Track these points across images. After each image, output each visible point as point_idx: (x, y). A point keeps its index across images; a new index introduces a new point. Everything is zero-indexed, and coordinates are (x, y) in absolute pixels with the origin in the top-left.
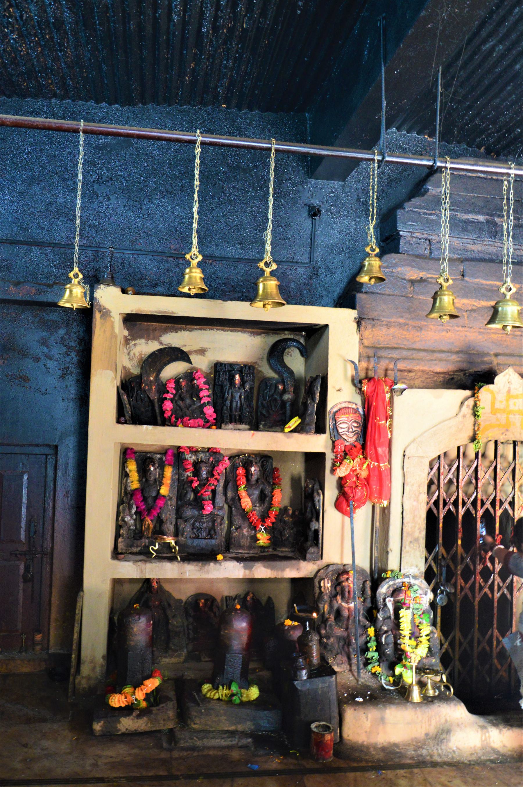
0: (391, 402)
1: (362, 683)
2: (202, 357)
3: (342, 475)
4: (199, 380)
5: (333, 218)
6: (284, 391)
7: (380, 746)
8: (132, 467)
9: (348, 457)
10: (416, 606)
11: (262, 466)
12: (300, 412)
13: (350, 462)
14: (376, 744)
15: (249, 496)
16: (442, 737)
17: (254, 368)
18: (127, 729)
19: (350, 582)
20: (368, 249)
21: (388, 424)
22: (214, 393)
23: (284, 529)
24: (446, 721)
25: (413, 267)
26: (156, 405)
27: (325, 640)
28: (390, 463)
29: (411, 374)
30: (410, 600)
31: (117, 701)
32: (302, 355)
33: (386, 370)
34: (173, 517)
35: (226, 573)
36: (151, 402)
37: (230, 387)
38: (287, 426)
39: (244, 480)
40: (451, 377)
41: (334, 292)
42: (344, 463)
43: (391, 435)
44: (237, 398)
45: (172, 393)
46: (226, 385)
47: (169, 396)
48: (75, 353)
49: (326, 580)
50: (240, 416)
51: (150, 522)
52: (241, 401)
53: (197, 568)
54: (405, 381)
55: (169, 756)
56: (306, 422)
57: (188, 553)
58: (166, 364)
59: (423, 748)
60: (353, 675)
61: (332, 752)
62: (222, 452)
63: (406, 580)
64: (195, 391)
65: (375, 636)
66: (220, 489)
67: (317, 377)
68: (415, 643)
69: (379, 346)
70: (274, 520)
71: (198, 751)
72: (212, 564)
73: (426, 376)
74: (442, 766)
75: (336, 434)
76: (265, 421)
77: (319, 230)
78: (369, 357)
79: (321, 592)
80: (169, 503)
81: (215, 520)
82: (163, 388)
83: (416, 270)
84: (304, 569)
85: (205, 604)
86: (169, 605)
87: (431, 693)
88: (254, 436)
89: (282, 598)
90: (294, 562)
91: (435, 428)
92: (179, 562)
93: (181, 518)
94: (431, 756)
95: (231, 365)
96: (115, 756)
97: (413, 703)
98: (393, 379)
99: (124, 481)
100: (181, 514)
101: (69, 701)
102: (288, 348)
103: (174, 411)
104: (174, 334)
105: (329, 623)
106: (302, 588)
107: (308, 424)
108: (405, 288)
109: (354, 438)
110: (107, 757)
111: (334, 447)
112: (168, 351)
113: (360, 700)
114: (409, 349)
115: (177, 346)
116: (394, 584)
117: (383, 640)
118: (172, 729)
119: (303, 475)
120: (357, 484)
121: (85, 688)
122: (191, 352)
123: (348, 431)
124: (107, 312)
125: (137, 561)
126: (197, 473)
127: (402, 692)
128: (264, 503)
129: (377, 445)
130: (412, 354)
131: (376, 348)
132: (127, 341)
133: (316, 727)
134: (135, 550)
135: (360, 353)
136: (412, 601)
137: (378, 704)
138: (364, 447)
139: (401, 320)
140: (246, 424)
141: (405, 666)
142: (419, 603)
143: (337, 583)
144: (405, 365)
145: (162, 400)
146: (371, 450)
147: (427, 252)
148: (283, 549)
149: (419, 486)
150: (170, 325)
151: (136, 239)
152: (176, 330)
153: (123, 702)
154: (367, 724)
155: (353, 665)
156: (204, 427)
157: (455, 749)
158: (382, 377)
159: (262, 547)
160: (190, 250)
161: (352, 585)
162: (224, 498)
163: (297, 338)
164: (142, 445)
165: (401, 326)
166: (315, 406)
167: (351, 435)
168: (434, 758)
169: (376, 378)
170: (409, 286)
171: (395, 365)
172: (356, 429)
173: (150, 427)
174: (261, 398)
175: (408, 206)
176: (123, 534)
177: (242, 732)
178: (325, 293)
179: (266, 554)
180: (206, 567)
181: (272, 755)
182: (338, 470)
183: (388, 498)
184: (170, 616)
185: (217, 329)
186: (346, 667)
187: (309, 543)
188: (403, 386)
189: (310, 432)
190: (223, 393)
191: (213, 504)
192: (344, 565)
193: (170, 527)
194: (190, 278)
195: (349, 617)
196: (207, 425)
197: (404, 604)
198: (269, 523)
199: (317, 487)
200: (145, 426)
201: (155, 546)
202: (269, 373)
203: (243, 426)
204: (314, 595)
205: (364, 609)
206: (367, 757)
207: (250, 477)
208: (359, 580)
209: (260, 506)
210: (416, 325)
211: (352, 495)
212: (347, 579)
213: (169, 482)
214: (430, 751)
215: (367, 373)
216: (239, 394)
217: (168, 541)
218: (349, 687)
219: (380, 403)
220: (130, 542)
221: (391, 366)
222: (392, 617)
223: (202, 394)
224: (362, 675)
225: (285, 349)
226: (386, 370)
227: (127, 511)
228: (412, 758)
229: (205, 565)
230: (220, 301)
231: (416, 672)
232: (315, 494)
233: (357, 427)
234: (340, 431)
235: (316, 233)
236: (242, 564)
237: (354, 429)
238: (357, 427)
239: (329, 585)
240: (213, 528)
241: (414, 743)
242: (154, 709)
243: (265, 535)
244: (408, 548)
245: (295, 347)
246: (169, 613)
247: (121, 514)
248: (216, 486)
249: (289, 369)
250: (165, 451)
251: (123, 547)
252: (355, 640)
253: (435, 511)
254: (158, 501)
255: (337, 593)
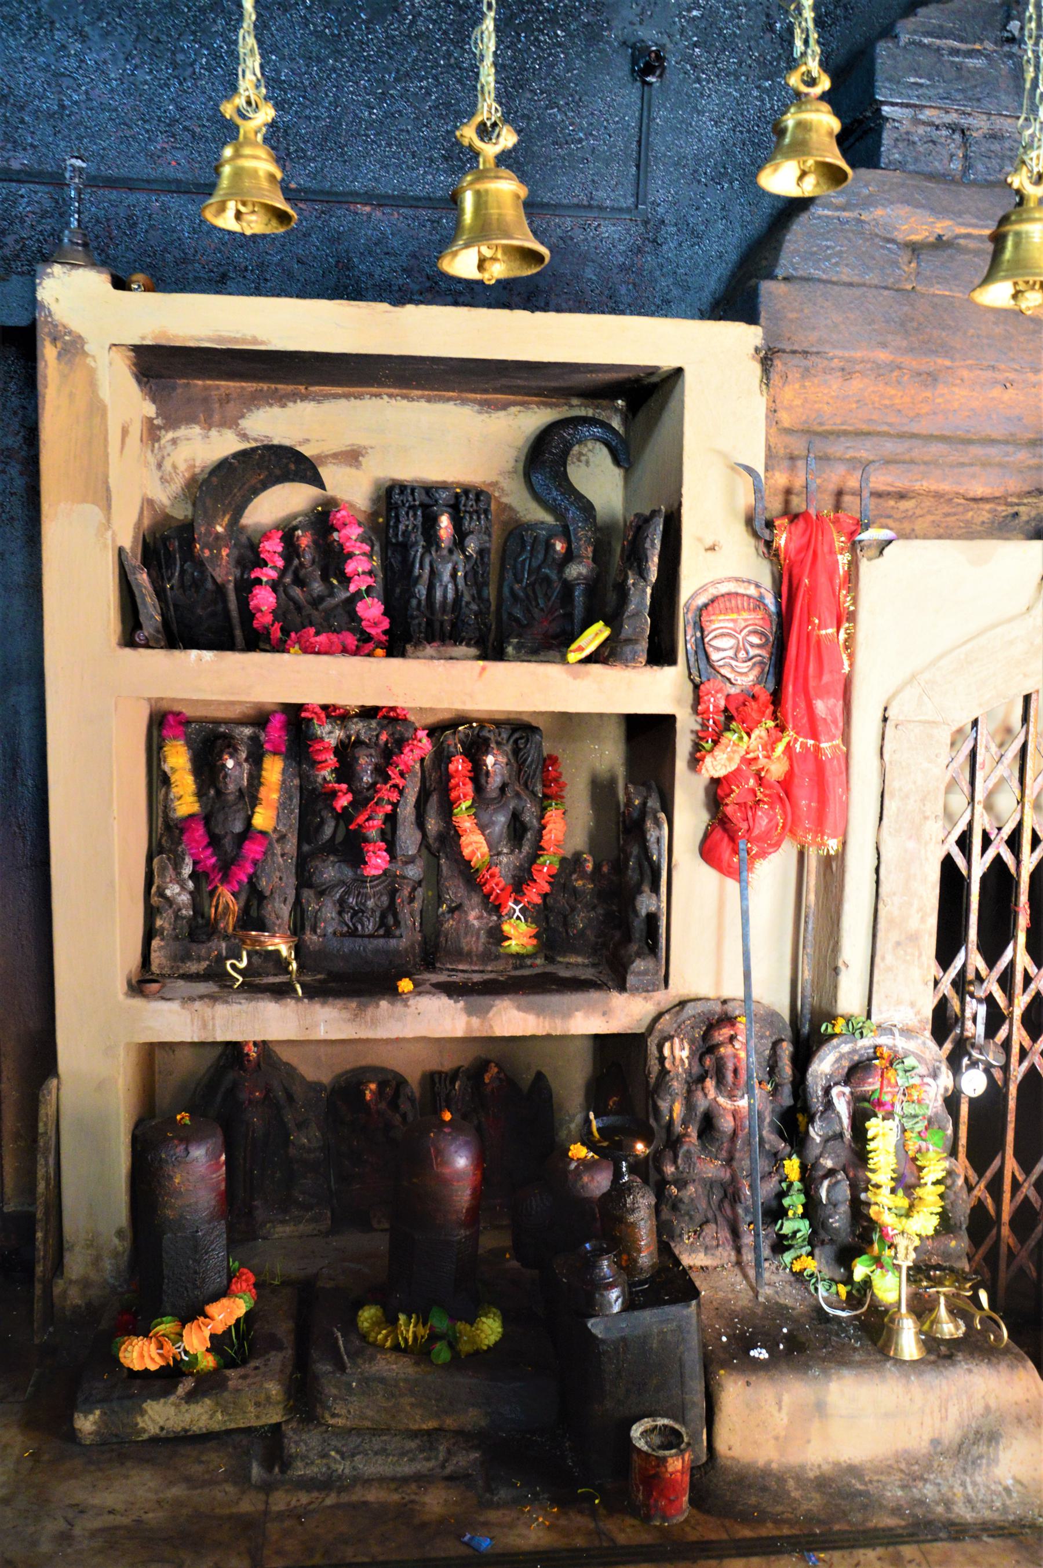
0: (852, 578)
1: (768, 1299)
2: (353, 471)
3: (720, 773)
4: (344, 532)
5: (698, 80)
6: (569, 556)
7: (811, 1475)
8: (178, 759)
9: (734, 725)
10: (910, 1109)
11: (516, 751)
12: (609, 610)
13: (741, 738)
14: (803, 1467)
15: (482, 828)
16: (976, 1451)
17: (489, 497)
18: (162, 1428)
19: (737, 1045)
20: (794, 80)
21: (842, 636)
22: (386, 566)
23: (573, 909)
24: (987, 1408)
25: (918, 206)
26: (232, 597)
27: (674, 1190)
28: (846, 739)
29: (904, 505)
30: (894, 1095)
31: (140, 1354)
32: (617, 462)
33: (840, 494)
34: (290, 882)
35: (427, 1021)
36: (220, 589)
37: (427, 549)
38: (573, 647)
39: (469, 788)
40: (1011, 510)
41: (701, 289)
42: (723, 741)
43: (851, 665)
44: (446, 578)
45: (274, 568)
46: (416, 543)
47: (268, 574)
48: (19, 467)
49: (676, 1040)
50: (454, 625)
51: (229, 897)
52: (456, 585)
53: (345, 1015)
54: (890, 522)
55: (261, 1507)
56: (623, 636)
57: (330, 974)
58: (256, 491)
59: (926, 1481)
60: (745, 1276)
61: (686, 1499)
62: (411, 717)
63: (884, 1040)
64: (333, 560)
65: (802, 1180)
66: (407, 812)
67: (654, 513)
68: (905, 1203)
69: (820, 429)
70: (547, 888)
71: (341, 1490)
72: (384, 1004)
73: (947, 509)
74: (976, 1538)
75: (703, 664)
76: (519, 636)
77: (660, 116)
78: (792, 458)
79: (664, 1072)
80: (278, 850)
81: (396, 890)
82: (250, 556)
83: (927, 213)
84: (623, 1012)
85: (380, 1092)
86: (290, 1097)
87: (949, 1328)
88: (486, 674)
89: (572, 1081)
90: (594, 995)
91: (969, 646)
92: (299, 1000)
93: (310, 886)
94: (948, 1504)
95: (430, 489)
96: (120, 1507)
97: (899, 1362)
98: (858, 516)
99: (161, 797)
100: (311, 875)
101: (37, 1341)
102: (579, 442)
103: (278, 613)
104: (276, 410)
105: (685, 1148)
106: (620, 1060)
107: (628, 641)
108: (895, 264)
109: (752, 677)
110: (100, 1511)
111: (697, 700)
112: (262, 456)
113: (760, 1354)
114: (902, 436)
115: (287, 443)
116: (854, 1051)
117: (823, 1194)
118: (278, 1425)
119: (621, 772)
120: (760, 796)
121: (79, 1307)
122: (323, 458)
123: (735, 658)
124: (73, 343)
125: (192, 999)
126: (346, 771)
127: (874, 1329)
128: (520, 846)
129: (812, 692)
130: (910, 449)
131: (812, 434)
132: (152, 432)
133: (644, 1433)
134: (194, 967)
135: (769, 448)
136: (900, 1096)
137: (809, 1367)
138: (777, 698)
139: (882, 356)
140: (468, 645)
141: (878, 1262)
142: (919, 1102)
143: (706, 1048)
144: (889, 479)
145: (246, 587)
146: (795, 705)
147: (956, 166)
148: (572, 959)
149: (923, 800)
150: (265, 386)
151: (163, 150)
152: (282, 400)
153: (152, 1359)
154: (781, 1419)
155: (744, 1251)
156: (356, 652)
157: (1010, 1482)
158: (827, 511)
159: (517, 956)
160: (234, 89)
161: (742, 1054)
162: (418, 836)
163: (602, 415)
164: (207, 703)
165: (879, 371)
166: (649, 590)
167: (744, 667)
168: (956, 1509)
169: (813, 512)
170: (906, 259)
171: (864, 479)
172: (757, 651)
173: (208, 655)
174: (509, 575)
175: (907, 30)
176: (162, 928)
177: (459, 1433)
178: (675, 292)
179: (526, 972)
180: (370, 1011)
181: (531, 1502)
182: (708, 760)
183: (840, 831)
184: (291, 1125)
185: (390, 396)
186: (727, 1254)
187: (634, 947)
188: (884, 534)
189: (634, 660)
190: (407, 566)
191: (391, 850)
192: (725, 1002)
193: (281, 910)
194: (238, 174)
195: (735, 1133)
196: (363, 644)
197: (880, 1103)
198: (533, 895)
199: (653, 803)
200: (194, 653)
201: (239, 958)
202: (536, 514)
203: (462, 650)
204: (647, 1077)
205: (773, 1111)
206: (779, 1508)
207: (483, 781)
208: (761, 1037)
209: (512, 852)
210: (923, 368)
211: (744, 826)
212: (732, 1039)
213: (275, 796)
214: (944, 1489)
215: (787, 502)
216: (450, 566)
217: (270, 948)
218: (733, 1314)
219: (823, 579)
220: (182, 949)
221: (853, 483)
222: (848, 1135)
223: (350, 567)
224: (766, 1275)
225: (572, 446)
226: (840, 494)
227: (170, 872)
228: (897, 1511)
229: (366, 1006)
230: (385, 306)
231: (908, 1280)
232: (649, 824)
233: (759, 646)
234: (714, 656)
235: (653, 126)
236: (461, 1004)
237: (753, 652)
238: (759, 646)
239: (685, 1054)
240: (392, 908)
241: (903, 1466)
242: (231, 1373)
243: (523, 927)
244: (889, 958)
245: (598, 439)
246: (288, 1117)
247: (157, 881)
248: (395, 805)
249: (580, 497)
250: (260, 718)
251: (164, 961)
252: (751, 1187)
253: (960, 861)
254: (247, 845)
255: (707, 1072)
